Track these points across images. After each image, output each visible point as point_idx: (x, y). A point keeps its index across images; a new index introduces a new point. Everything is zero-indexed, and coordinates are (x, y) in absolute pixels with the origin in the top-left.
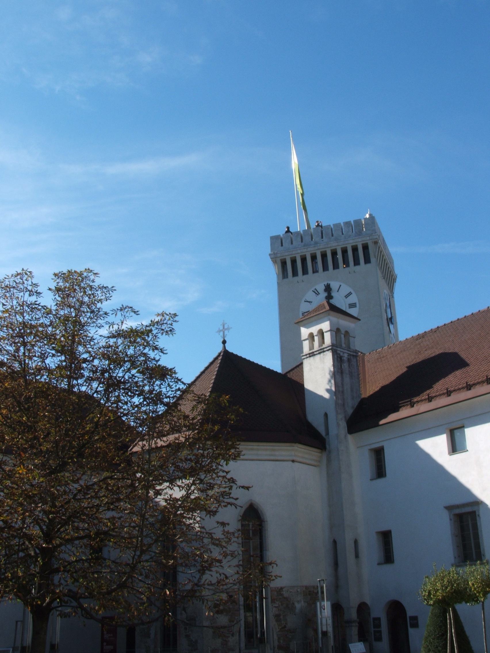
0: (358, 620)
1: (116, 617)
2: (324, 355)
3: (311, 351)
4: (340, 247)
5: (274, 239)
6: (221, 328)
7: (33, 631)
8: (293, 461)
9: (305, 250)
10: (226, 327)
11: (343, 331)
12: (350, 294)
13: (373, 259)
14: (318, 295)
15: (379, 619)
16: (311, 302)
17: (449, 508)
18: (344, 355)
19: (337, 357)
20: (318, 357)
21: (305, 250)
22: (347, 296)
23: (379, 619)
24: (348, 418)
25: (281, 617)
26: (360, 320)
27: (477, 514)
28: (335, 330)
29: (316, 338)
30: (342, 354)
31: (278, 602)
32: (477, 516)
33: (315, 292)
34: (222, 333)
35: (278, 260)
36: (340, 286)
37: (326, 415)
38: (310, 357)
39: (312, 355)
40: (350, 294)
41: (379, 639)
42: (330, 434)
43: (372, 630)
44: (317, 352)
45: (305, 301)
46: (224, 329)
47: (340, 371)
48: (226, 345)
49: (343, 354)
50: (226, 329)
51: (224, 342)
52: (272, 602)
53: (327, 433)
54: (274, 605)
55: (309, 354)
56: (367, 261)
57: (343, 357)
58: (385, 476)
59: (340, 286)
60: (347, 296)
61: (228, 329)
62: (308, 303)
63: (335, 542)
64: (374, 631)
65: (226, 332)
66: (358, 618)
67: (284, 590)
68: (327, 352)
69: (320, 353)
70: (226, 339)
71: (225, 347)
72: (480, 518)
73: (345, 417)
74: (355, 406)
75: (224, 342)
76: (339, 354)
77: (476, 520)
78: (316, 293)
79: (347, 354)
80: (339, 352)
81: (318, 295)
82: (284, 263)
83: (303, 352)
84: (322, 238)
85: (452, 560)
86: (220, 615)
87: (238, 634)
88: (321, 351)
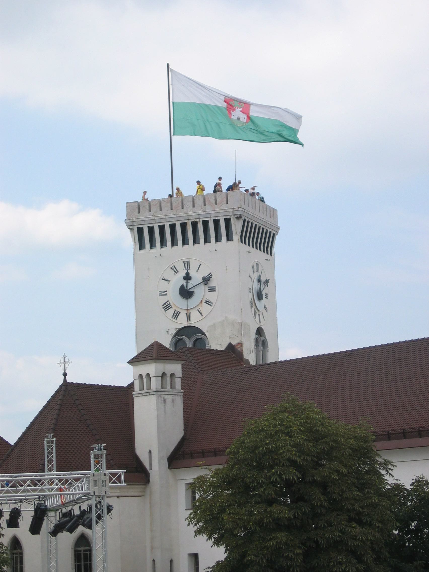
1: (308, 499)
4: (201, 220)
5: (129, 205)
8: (118, 497)
10: (66, 360)
11: (169, 375)
14: (176, 273)
29: (145, 380)
33: (184, 264)
34: (63, 365)
35: (135, 228)
36: (200, 264)
37: (150, 452)
39: (141, 395)
51: (65, 375)
53: (151, 469)
59: (200, 264)
61: (69, 362)
63: (154, 561)
65: (67, 365)
68: (152, 395)
70: (66, 371)
71: (65, 379)
75: (65, 375)
78: (175, 271)
81: (176, 273)
82: (140, 231)
88: (148, 394)
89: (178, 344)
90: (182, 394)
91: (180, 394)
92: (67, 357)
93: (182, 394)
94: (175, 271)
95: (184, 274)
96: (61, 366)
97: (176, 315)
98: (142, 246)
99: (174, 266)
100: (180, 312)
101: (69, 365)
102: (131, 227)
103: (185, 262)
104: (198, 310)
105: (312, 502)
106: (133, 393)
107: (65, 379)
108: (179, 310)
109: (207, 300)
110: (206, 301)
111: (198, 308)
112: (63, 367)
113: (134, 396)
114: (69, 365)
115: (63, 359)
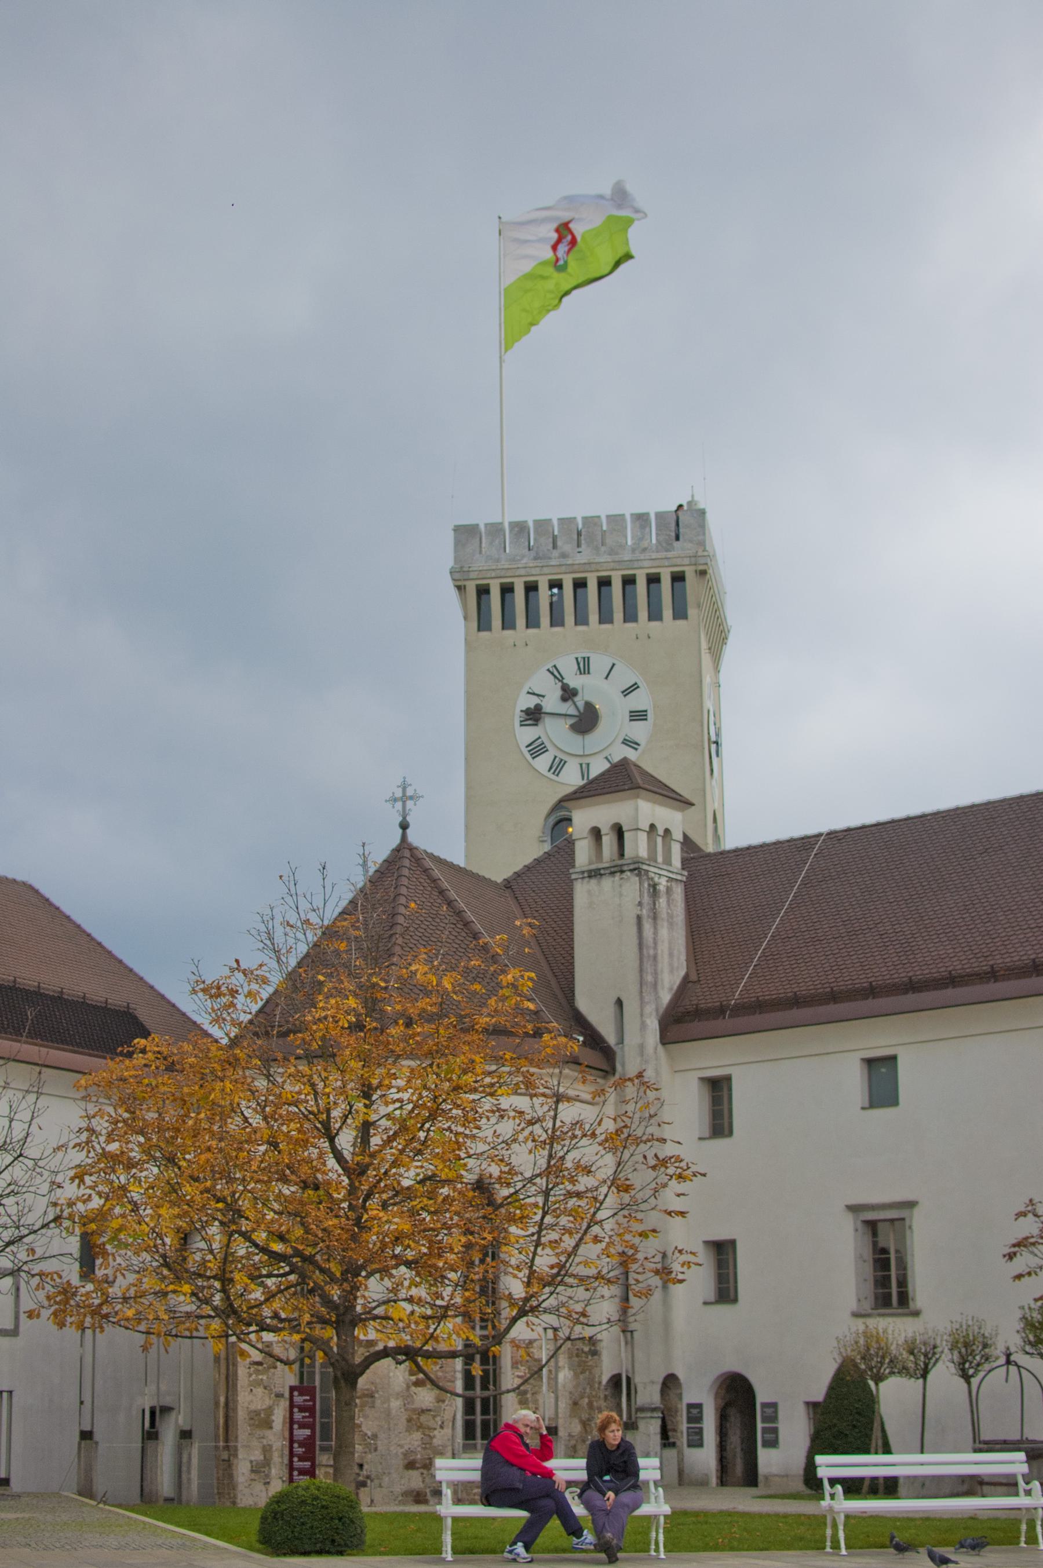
0: (662, 1406)
2: (622, 879)
3: (593, 867)
6: (399, 794)
7: (926, 1477)
9: (536, 571)
10: (410, 792)
12: (635, 687)
13: (692, 612)
15: (699, 1406)
16: (543, 696)
17: (854, 1209)
18: (660, 881)
19: (649, 885)
20: (607, 883)
21: (536, 571)
22: (627, 692)
23: (699, 1406)
24: (661, 1011)
25: (529, 1396)
26: (692, 805)
27: (907, 1223)
28: (648, 829)
29: (606, 840)
30: (656, 879)
31: (523, 1368)
32: (907, 1227)
33: (552, 674)
34: (399, 805)
36: (614, 665)
37: (619, 1003)
38: (590, 877)
39: (594, 874)
40: (635, 687)
41: (696, 1441)
42: (626, 1042)
43: (684, 1426)
44: (608, 871)
45: (529, 693)
46: (405, 798)
47: (651, 914)
48: (408, 831)
49: (659, 878)
50: (411, 798)
51: (404, 826)
52: (512, 1367)
53: (621, 1041)
54: (517, 1374)
55: (590, 871)
56: (680, 613)
57: (659, 884)
58: (730, 1133)
59: (614, 665)
60: (627, 692)
62: (536, 692)
64: (688, 1428)
66: (661, 1403)
67: (535, 1345)
69: (613, 873)
70: (408, 818)
71: (404, 837)
72: (912, 1232)
73: (657, 1010)
74: (675, 987)
75: (404, 826)
76: (652, 879)
77: (904, 1237)
79: (667, 879)
80: (651, 875)
81: (581, 673)
82: (483, 591)
83: (574, 866)
84: (579, 545)
85: (853, 1305)
86: (420, 1389)
87: (451, 1424)
89: (561, 824)
90: (684, 879)
91: (679, 877)
92: (410, 785)
93: (684, 879)
94: (555, 677)
95: (559, 693)
96: (393, 807)
97: (557, 766)
98: (483, 624)
99: (555, 666)
100: (565, 762)
101: (415, 805)
102: (459, 583)
103: (579, 660)
104: (606, 758)
105: (333, 1351)
106: (571, 871)
107: (404, 837)
108: (564, 757)
109: (627, 738)
110: (625, 739)
111: (605, 754)
112: (400, 809)
113: (573, 877)
114: (415, 805)
115: (400, 790)
